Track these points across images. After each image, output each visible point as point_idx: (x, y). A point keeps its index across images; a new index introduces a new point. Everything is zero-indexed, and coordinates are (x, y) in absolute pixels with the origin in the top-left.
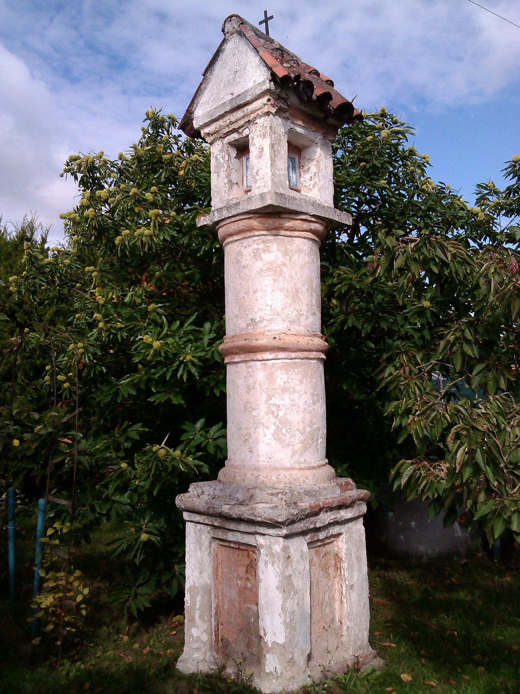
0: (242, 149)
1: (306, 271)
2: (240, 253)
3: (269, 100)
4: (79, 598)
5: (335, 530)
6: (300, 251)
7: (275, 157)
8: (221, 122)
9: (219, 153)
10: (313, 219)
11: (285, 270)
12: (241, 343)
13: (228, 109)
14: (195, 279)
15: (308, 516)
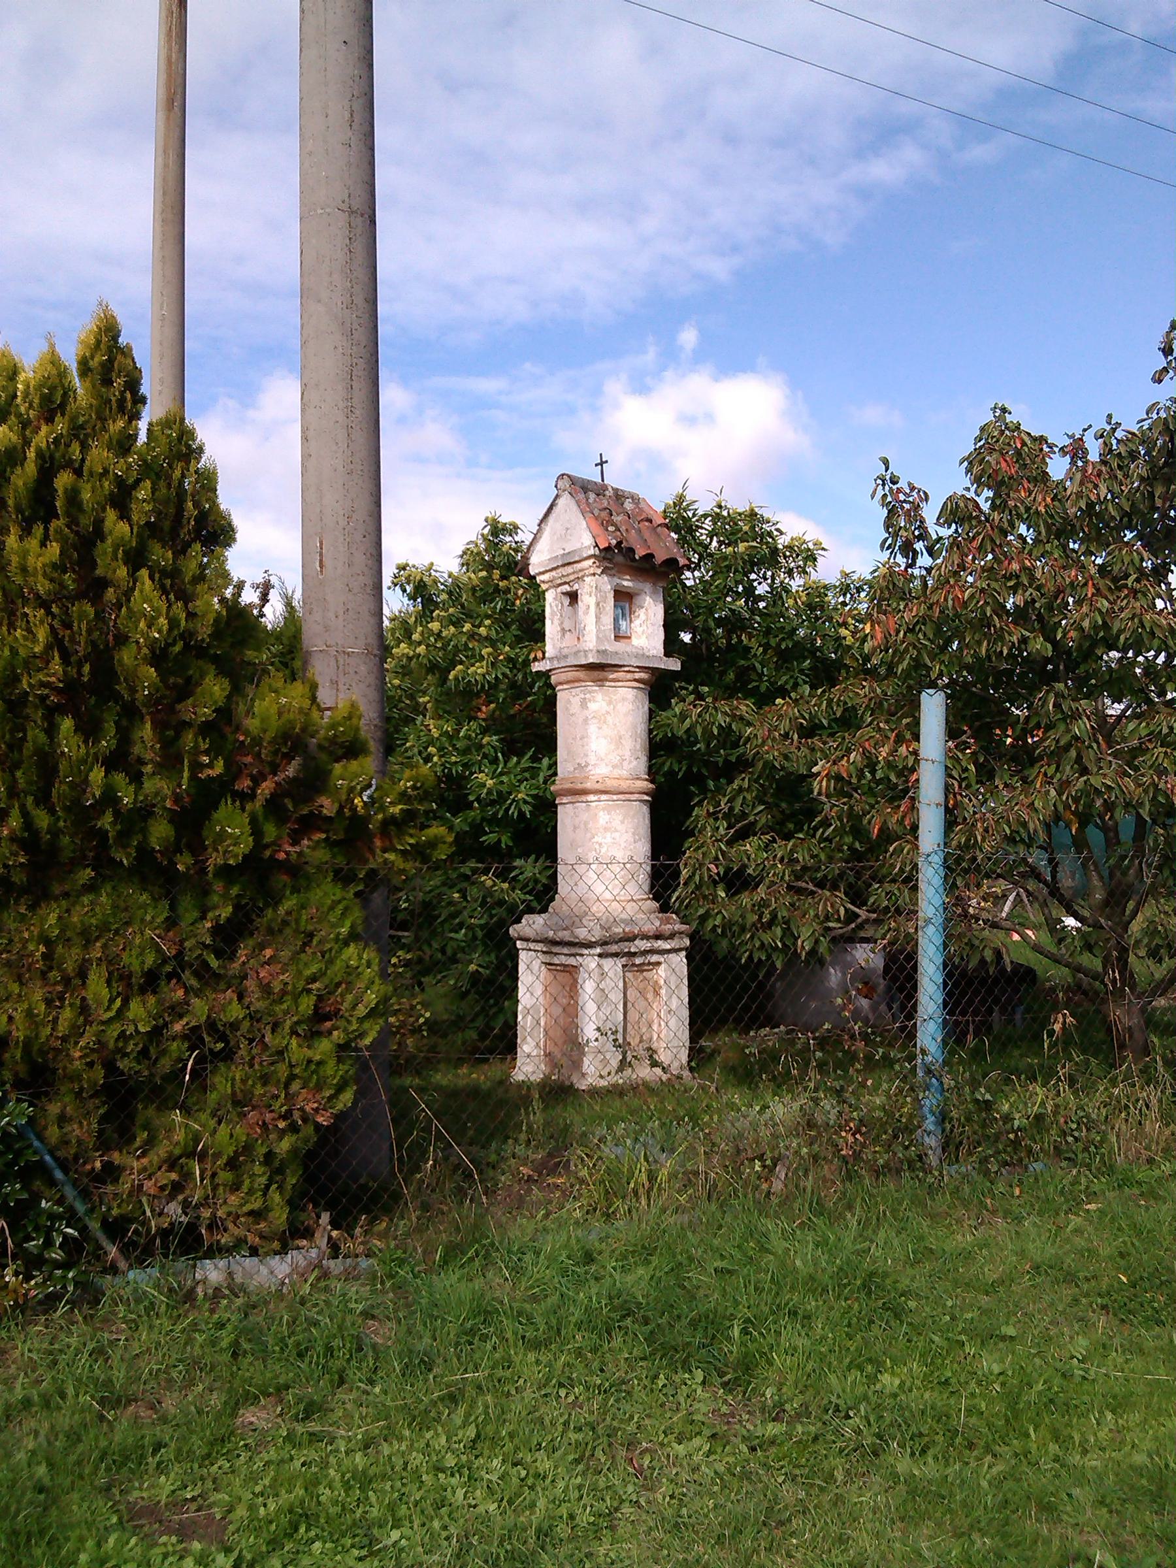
0: (573, 597)
1: (630, 718)
2: (569, 702)
4: (422, 1020)
5: (655, 958)
6: (624, 699)
8: (554, 573)
9: (552, 601)
11: (609, 718)
12: (568, 786)
14: (531, 727)
15: (621, 940)
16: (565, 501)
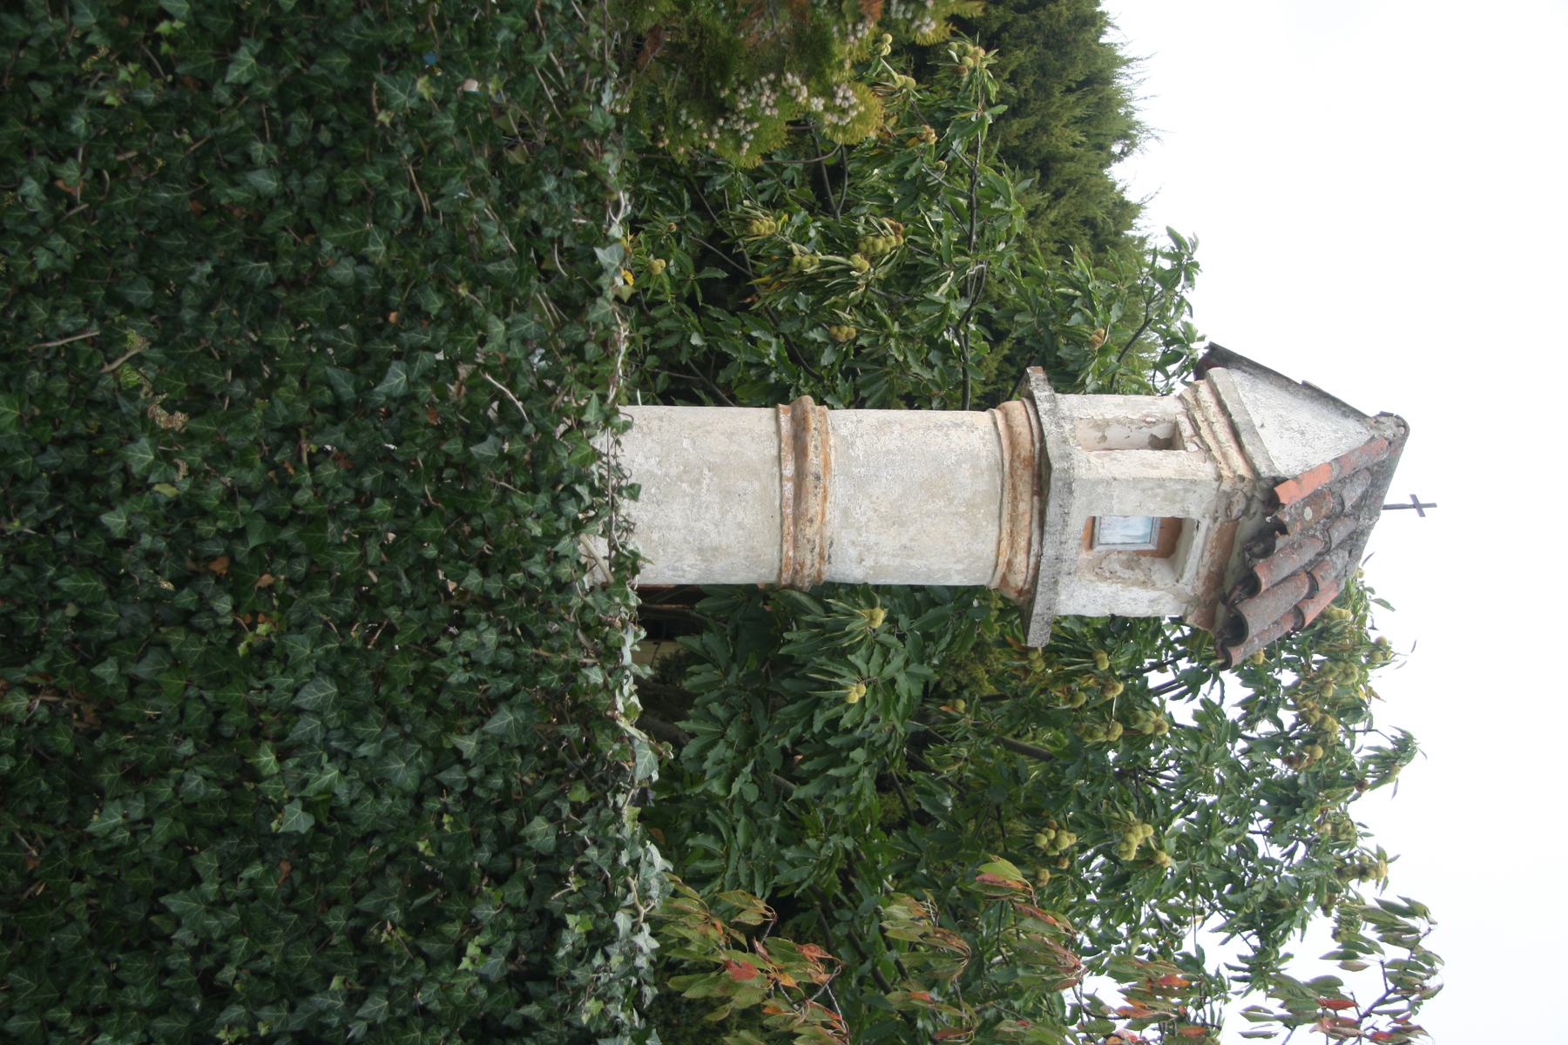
0: (1170, 442)
3: (1242, 479)
7: (1143, 490)
8: (1213, 408)
10: (1033, 560)
13: (1236, 418)
16: (1351, 436)
